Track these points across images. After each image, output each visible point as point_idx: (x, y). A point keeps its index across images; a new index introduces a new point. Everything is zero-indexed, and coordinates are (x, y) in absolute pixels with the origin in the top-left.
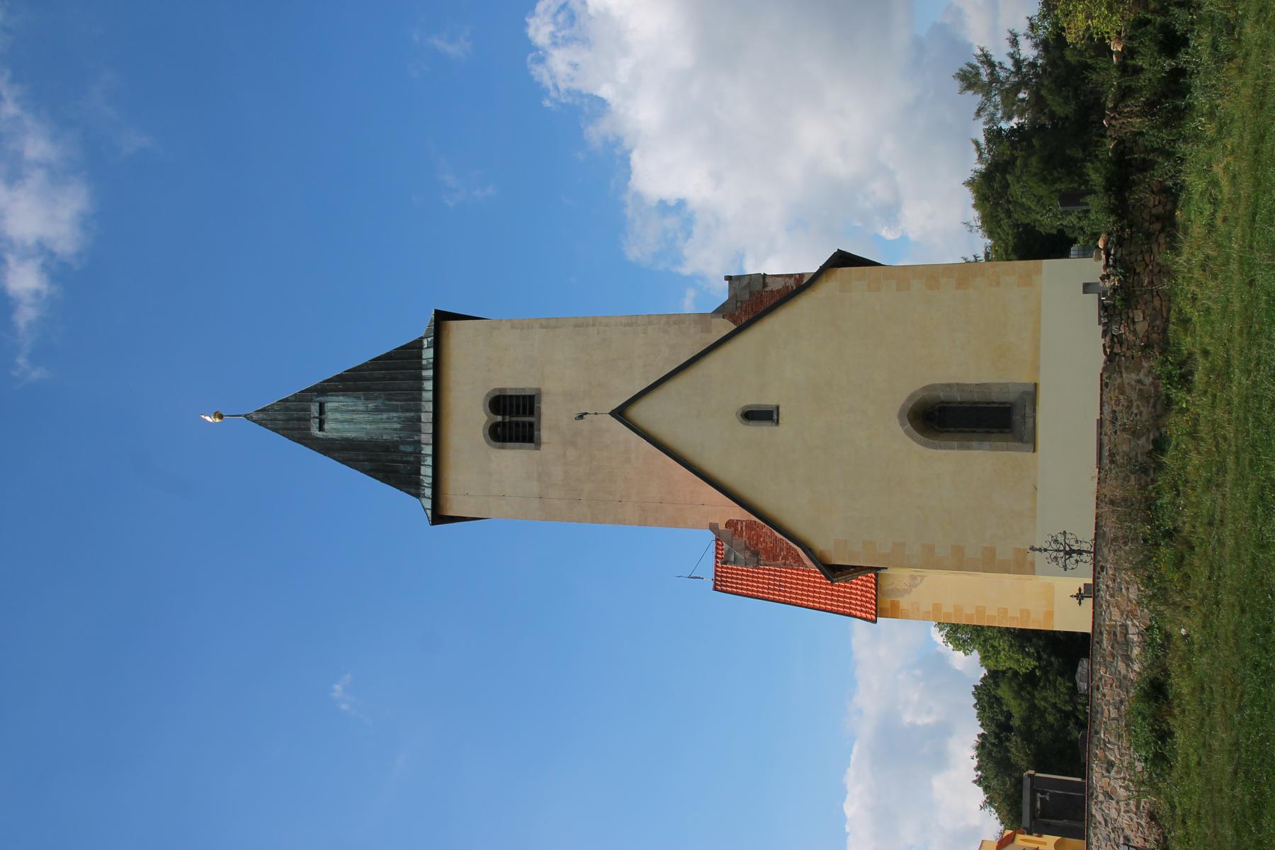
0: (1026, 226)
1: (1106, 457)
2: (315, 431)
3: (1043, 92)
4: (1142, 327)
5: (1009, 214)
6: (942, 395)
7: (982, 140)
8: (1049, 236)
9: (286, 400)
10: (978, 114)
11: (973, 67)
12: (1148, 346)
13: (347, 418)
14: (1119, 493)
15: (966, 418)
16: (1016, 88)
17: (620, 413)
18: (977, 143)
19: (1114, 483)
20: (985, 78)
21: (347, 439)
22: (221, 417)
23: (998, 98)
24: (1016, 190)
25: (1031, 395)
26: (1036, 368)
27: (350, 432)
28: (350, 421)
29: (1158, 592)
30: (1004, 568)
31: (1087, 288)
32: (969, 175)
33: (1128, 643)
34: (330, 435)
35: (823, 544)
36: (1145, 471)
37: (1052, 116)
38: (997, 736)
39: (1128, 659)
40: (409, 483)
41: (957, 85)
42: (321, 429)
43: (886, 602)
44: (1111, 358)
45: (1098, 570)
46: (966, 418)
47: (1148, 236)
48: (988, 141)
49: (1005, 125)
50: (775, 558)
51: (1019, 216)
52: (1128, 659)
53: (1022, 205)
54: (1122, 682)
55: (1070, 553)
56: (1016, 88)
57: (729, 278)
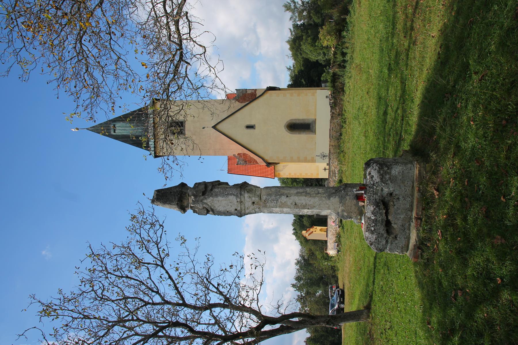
0: (306, 59)
1: (331, 137)
2: (112, 133)
3: (311, 15)
4: (338, 111)
5: (301, 54)
6: (294, 122)
7: (292, 29)
8: (314, 62)
9: (101, 124)
10: (290, 19)
11: (289, 3)
12: (339, 115)
13: (121, 129)
14: (333, 144)
15: (299, 127)
16: (303, 11)
17: (214, 127)
18: (290, 30)
19: (149, 87)
20: (293, 7)
21: (124, 135)
22: (78, 129)
23: (297, 14)
24: (303, 47)
25: (315, 121)
26: (316, 115)
27: (125, 133)
28: (125, 130)
29: (340, 162)
30: (309, 162)
31: (327, 97)
32: (287, 39)
33: (335, 173)
34: (118, 134)
35: (266, 158)
36: (338, 139)
37: (314, 21)
38: (299, 219)
39: (335, 176)
40: (147, 148)
41: (284, 9)
42: (114, 132)
43: (277, 173)
44: (332, 117)
45: (330, 159)
46: (299, 127)
47: (339, 92)
48: (294, 28)
49: (299, 23)
50: (251, 162)
51: (304, 56)
52: (335, 176)
53: (305, 52)
54: (334, 181)
55: (324, 156)
56: (303, 11)
57: (236, 90)
